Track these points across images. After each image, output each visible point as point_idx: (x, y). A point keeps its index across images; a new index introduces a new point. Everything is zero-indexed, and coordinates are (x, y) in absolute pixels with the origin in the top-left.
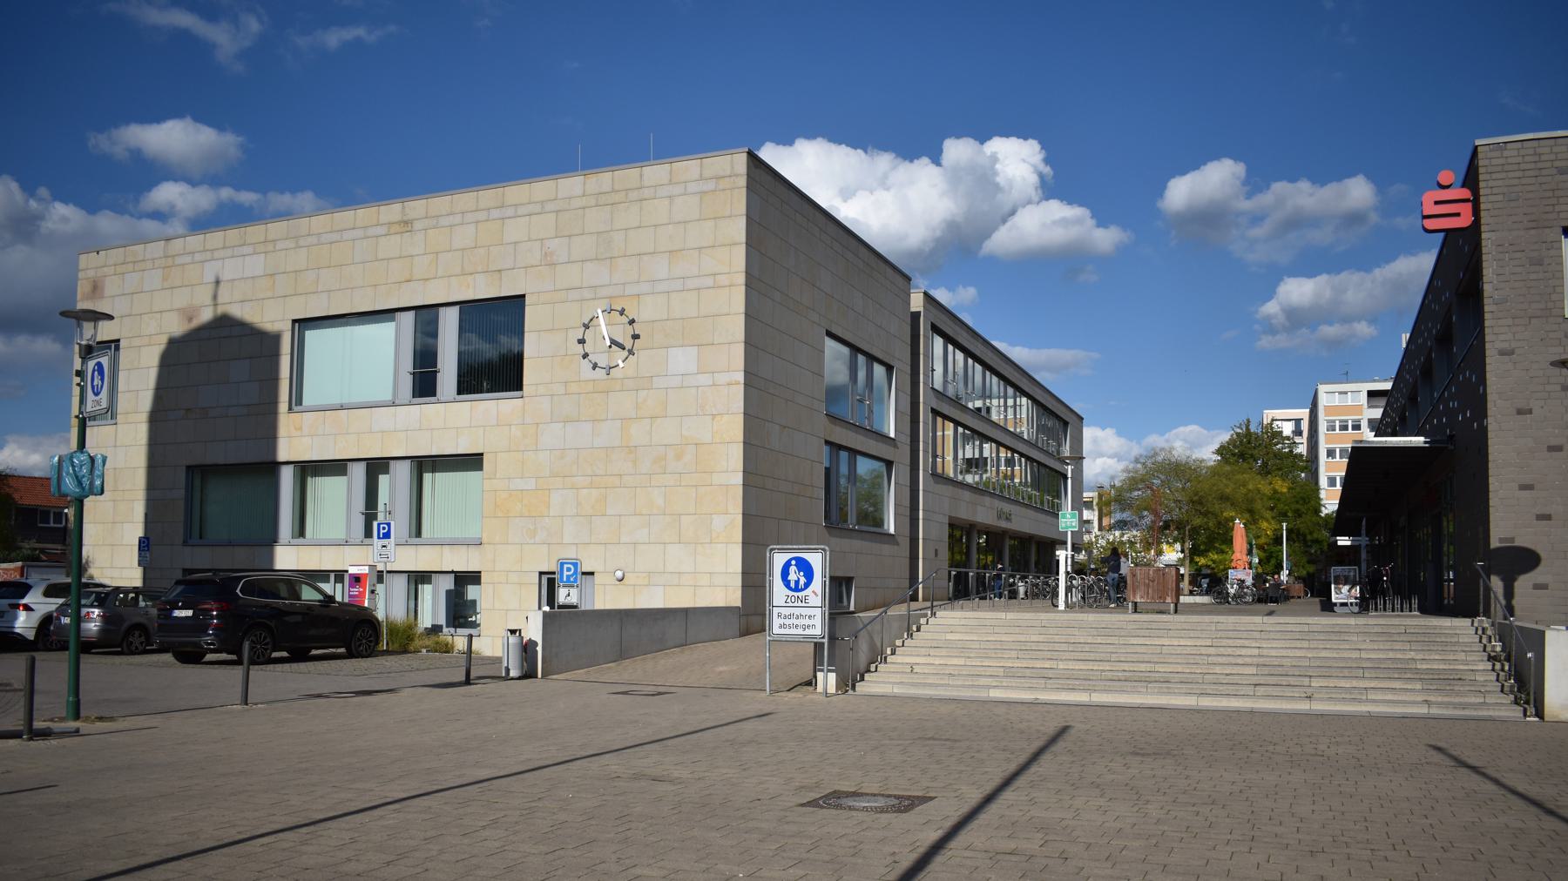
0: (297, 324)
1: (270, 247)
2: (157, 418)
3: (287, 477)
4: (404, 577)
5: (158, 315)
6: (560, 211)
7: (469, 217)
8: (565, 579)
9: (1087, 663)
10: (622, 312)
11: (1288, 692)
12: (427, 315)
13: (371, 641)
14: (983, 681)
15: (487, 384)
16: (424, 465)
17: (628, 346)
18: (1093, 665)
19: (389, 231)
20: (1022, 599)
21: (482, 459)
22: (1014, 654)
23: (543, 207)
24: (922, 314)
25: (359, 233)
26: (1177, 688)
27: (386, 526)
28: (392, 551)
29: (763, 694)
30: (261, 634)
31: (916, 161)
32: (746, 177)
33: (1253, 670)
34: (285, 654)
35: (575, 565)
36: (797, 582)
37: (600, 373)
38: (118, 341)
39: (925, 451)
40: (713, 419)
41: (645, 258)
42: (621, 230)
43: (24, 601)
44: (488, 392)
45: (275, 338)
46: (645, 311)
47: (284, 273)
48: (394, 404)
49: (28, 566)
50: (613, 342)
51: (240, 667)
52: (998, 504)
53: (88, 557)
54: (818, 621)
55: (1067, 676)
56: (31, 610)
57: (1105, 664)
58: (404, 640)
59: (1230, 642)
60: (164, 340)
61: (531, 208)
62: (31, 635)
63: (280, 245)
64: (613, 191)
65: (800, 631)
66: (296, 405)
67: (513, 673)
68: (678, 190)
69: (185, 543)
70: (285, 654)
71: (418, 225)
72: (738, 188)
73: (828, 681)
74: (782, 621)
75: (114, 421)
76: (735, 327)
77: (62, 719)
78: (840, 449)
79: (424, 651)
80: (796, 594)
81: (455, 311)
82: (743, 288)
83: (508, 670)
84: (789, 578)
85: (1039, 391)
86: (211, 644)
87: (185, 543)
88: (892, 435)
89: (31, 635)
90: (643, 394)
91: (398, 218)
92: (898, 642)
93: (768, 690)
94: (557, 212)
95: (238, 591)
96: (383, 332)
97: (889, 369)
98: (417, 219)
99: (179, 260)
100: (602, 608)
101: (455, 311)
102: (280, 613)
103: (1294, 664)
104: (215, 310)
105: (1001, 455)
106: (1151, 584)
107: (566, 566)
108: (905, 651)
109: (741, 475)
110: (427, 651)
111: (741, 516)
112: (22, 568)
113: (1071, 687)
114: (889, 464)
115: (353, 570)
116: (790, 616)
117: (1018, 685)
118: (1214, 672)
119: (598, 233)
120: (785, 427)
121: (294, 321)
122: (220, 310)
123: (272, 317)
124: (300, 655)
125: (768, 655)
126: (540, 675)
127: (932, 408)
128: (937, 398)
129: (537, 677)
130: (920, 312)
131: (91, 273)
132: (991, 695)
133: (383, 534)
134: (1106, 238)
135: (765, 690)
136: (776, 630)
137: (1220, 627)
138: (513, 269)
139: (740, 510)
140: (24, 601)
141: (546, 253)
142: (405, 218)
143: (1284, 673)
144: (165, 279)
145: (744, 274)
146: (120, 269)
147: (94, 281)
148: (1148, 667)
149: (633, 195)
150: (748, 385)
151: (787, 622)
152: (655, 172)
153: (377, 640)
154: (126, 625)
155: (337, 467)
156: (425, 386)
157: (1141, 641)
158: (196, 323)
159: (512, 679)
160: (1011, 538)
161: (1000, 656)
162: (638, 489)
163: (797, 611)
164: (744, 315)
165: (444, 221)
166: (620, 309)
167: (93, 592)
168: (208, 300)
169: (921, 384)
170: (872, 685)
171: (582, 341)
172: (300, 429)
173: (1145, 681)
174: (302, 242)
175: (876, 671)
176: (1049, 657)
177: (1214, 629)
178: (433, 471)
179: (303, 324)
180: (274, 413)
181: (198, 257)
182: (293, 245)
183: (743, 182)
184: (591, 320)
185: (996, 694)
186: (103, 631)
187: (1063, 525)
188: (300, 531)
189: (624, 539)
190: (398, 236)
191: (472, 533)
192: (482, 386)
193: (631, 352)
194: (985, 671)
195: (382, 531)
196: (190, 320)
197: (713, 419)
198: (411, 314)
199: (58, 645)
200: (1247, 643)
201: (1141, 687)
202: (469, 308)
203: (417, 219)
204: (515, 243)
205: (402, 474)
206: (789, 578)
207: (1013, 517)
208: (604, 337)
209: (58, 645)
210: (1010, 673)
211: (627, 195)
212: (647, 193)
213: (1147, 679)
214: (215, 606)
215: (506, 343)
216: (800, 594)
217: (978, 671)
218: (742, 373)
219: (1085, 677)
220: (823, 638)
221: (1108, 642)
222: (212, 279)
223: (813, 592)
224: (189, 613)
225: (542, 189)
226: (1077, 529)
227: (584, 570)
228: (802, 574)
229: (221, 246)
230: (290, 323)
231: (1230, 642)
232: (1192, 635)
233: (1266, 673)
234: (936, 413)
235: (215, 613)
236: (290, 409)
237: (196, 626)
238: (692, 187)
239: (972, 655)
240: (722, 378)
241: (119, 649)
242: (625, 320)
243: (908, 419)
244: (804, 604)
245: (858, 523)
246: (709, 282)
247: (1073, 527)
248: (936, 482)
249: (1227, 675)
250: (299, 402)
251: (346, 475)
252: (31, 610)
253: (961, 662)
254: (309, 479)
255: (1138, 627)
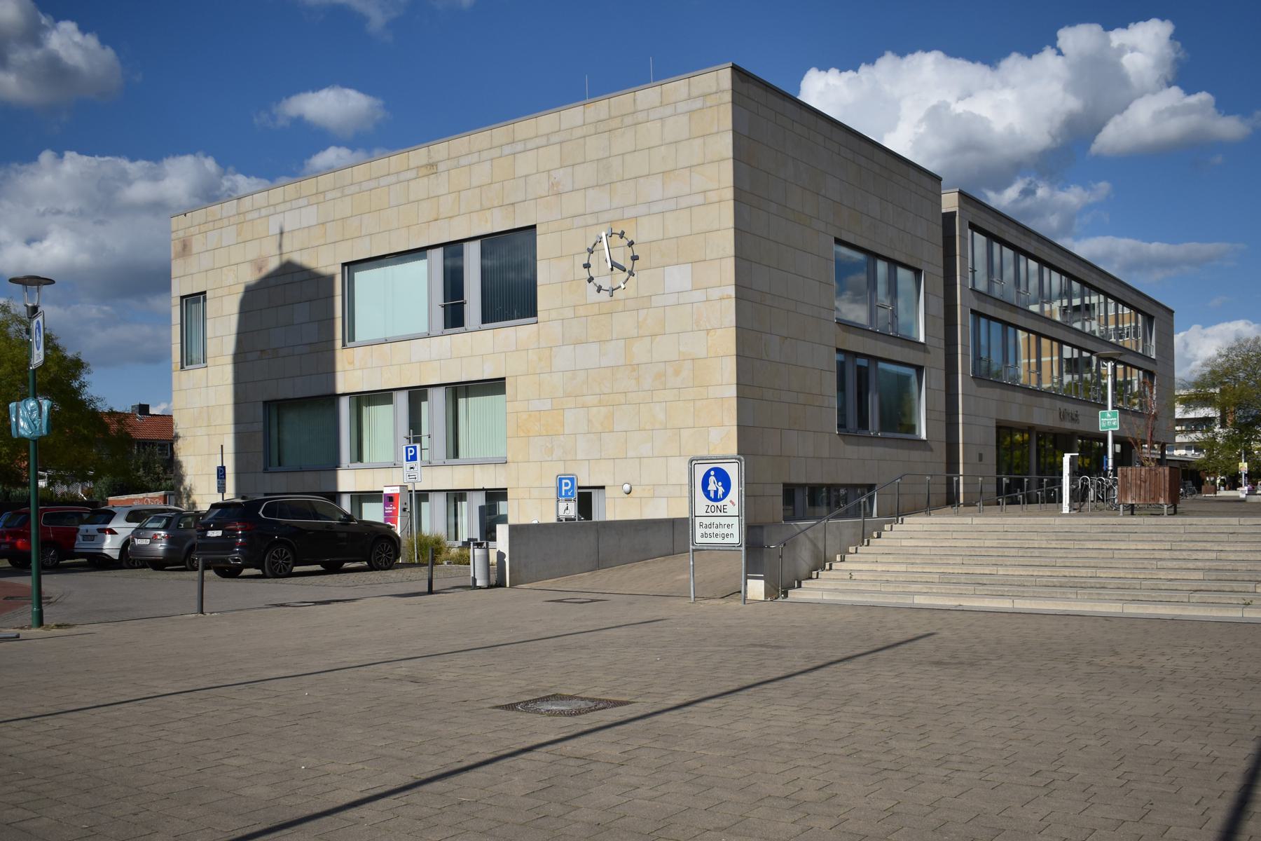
0: (346, 267)
1: (321, 198)
2: (239, 358)
3: (345, 405)
4: (443, 496)
5: (234, 267)
6: (563, 142)
7: (485, 155)
8: (563, 494)
9: (1028, 568)
10: (622, 235)
11: (1225, 598)
12: (453, 249)
13: (390, 555)
14: (914, 588)
15: (518, 312)
16: (458, 391)
17: (628, 268)
18: (1033, 571)
19: (418, 174)
20: (1092, 501)
21: (505, 383)
22: (959, 560)
23: (548, 140)
24: (957, 214)
25: (393, 179)
26: (1107, 594)
27: (413, 449)
28: (419, 472)
29: (682, 603)
30: (282, 551)
31: (1035, 57)
32: (731, 91)
33: (1199, 575)
34: (318, 567)
35: (572, 480)
36: (716, 492)
37: (604, 295)
38: (204, 293)
39: (965, 354)
40: (708, 334)
41: (641, 180)
42: (619, 155)
43: (109, 526)
44: (518, 318)
45: (331, 279)
46: (643, 233)
47: (333, 221)
48: (429, 336)
49: (170, 495)
50: (614, 265)
51: (30, 577)
52: (1059, 404)
53: (191, 485)
54: (735, 530)
55: (1002, 582)
56: (116, 533)
57: (1046, 569)
58: (431, 552)
59: (1191, 545)
60: (241, 289)
61: (539, 142)
62: (115, 555)
63: (329, 195)
64: (610, 118)
65: (719, 540)
66: (349, 341)
67: (479, 583)
68: (668, 110)
69: (266, 470)
70: (318, 567)
71: (442, 167)
72: (724, 104)
73: (756, 588)
74: (703, 530)
75: (205, 365)
76: (726, 242)
77: (30, 627)
78: (856, 357)
79: (445, 563)
80: (716, 504)
81: (477, 244)
82: (732, 203)
83: (474, 580)
84: (709, 489)
85: (1113, 286)
86: (238, 560)
87: (266, 470)
88: (922, 339)
89: (115, 555)
90: (643, 313)
91: (424, 161)
92: (852, 549)
93: (692, 597)
94: (561, 143)
95: (260, 513)
96: (418, 268)
97: (917, 272)
98: (441, 161)
99: (249, 216)
100: (613, 519)
101: (477, 244)
102: (329, 532)
103: (1249, 568)
104: (281, 258)
105: (1043, 359)
106: (1143, 484)
107: (564, 481)
108: (860, 558)
109: (734, 387)
110: (448, 563)
111: (735, 428)
112: (165, 496)
113: (1000, 593)
114: (919, 369)
115: (387, 491)
116: (710, 526)
117: (948, 591)
118: (1159, 577)
119: (598, 160)
120: (786, 338)
121: (344, 265)
122: (285, 258)
123: (326, 262)
124: (333, 568)
125: (691, 563)
126: (508, 585)
127: (971, 310)
128: (978, 299)
129: (505, 586)
130: (955, 212)
131: (181, 234)
132: (915, 602)
133: (411, 456)
134: (1230, 127)
135: (690, 597)
136: (699, 539)
137: (1192, 529)
138: (525, 201)
139: (735, 422)
140: (109, 526)
141: (552, 184)
142: (431, 161)
143: (1233, 578)
144: (238, 234)
145: (732, 189)
146: (203, 228)
147: (184, 240)
148: (1090, 572)
149: (629, 120)
150: (739, 298)
151: (708, 531)
152: (647, 96)
153: (397, 555)
154: (187, 545)
155: (383, 397)
156: (454, 317)
157: (1097, 545)
158: (264, 272)
159: (480, 588)
160: (1082, 438)
161: (945, 562)
162: (641, 405)
163: (717, 521)
164: (733, 230)
165: (464, 161)
166: (620, 232)
167: (164, 517)
168: (275, 251)
169: (958, 286)
170: (808, 592)
171: (587, 266)
172: (352, 363)
173: (1076, 586)
174: (347, 191)
175: (817, 578)
176: (994, 562)
177: (1182, 531)
178: (467, 396)
179: (351, 266)
180: (332, 350)
181: (264, 212)
182: (339, 195)
183: (728, 97)
184: (595, 244)
185: (920, 601)
186: (167, 550)
187: (1104, 425)
188: (359, 457)
189: (630, 454)
190: (426, 179)
191: (500, 453)
192: (513, 313)
193: (631, 273)
194: (921, 577)
195: (410, 454)
196: (260, 269)
197: (708, 334)
198: (440, 251)
199: (140, 564)
200: (1208, 546)
201: (1071, 593)
202: (489, 241)
203: (441, 161)
204: (526, 176)
205: (437, 399)
206: (709, 489)
207: (1080, 418)
208: (606, 260)
209: (140, 564)
210: (945, 579)
211: (622, 121)
212: (641, 117)
213: (1083, 585)
214: (239, 527)
215: (527, 275)
216: (719, 504)
217: (915, 577)
218: (733, 287)
219: (1020, 583)
220: (741, 546)
221: (1063, 546)
222: (278, 231)
223: (731, 501)
224: (219, 533)
225: (546, 122)
226: (1118, 429)
227: (580, 485)
228: (720, 484)
229: (281, 200)
230: (340, 266)
231: (1191, 545)
232: (1155, 539)
233: (1214, 578)
234: (977, 314)
235: (240, 532)
236: (344, 345)
237: (224, 544)
238: (682, 107)
239: (918, 561)
240: (715, 293)
241: (184, 567)
242: (624, 242)
243: (942, 322)
244: (723, 514)
245: (882, 429)
246: (699, 199)
247: (1112, 426)
248: (979, 386)
249: (1171, 580)
250: (352, 338)
251: (392, 404)
252: (116, 533)
253: (903, 568)
254: (364, 408)
255: (1102, 530)
